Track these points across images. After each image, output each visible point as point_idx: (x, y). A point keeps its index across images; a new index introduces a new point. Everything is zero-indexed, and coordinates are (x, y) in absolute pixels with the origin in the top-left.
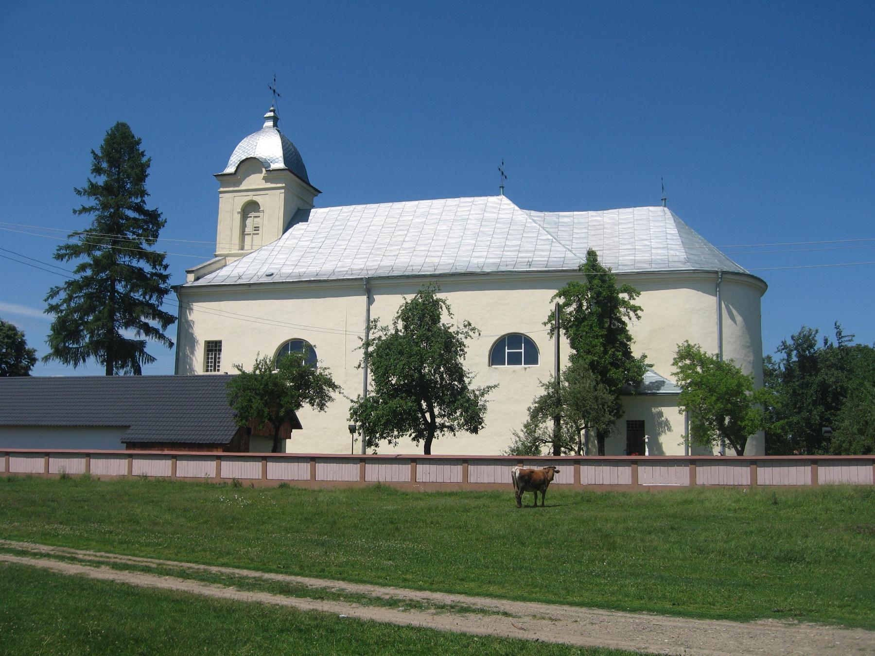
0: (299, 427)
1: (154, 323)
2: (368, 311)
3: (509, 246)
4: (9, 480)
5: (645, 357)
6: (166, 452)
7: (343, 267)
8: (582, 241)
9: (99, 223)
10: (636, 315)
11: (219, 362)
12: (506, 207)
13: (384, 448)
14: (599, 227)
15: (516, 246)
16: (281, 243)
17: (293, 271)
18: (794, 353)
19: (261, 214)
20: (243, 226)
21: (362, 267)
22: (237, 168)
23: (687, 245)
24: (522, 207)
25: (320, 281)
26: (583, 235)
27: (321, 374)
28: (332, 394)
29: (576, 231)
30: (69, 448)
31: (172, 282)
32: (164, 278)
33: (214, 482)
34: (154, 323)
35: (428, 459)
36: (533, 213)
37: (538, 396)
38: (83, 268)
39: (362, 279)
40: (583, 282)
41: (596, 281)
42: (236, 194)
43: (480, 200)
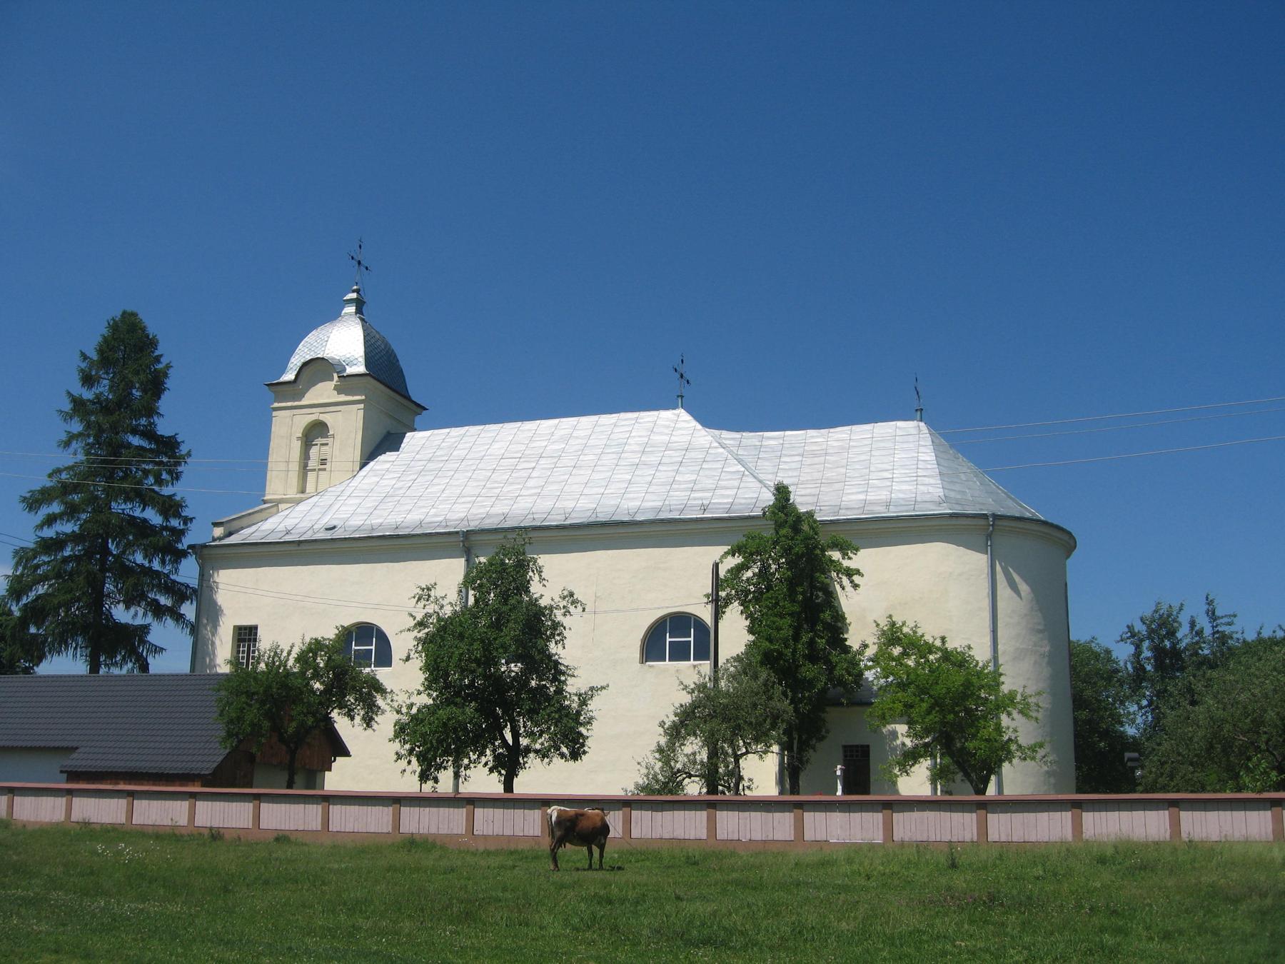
0: (346, 753)
3: (680, 483)
4: (277, 839)
6: (121, 787)
8: (790, 474)
10: (852, 582)
12: (687, 425)
15: (690, 482)
18: (1146, 644)
19: (330, 440)
20: (305, 456)
21: (462, 515)
25: (398, 536)
33: (184, 832)
34: (165, 601)
35: (509, 801)
38: (50, 520)
40: (769, 533)
42: (296, 411)
43: (648, 417)
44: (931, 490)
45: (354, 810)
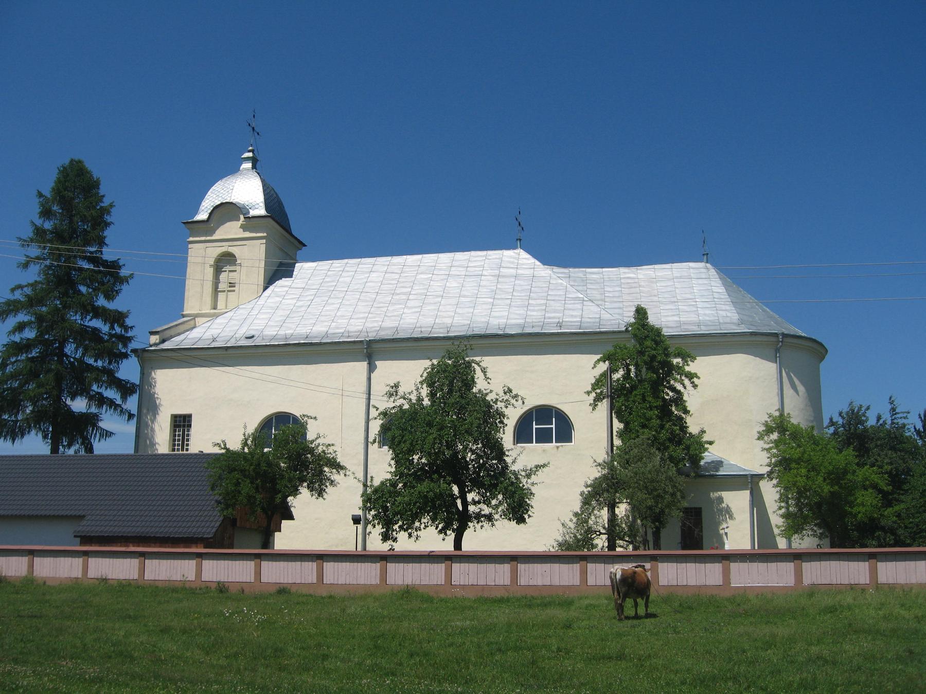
0: (291, 517)
1: (111, 393)
2: (369, 379)
5: (703, 432)
6: (132, 549)
7: (338, 328)
9: (46, 274)
10: (693, 383)
11: (188, 440)
12: (525, 261)
13: (404, 543)
16: (262, 301)
17: (282, 333)
19: (238, 268)
21: (360, 328)
22: (211, 214)
24: (544, 264)
25: (311, 344)
26: (617, 294)
27: (324, 452)
28: (335, 477)
29: (607, 289)
30: (8, 544)
31: (133, 345)
32: (126, 340)
33: (193, 586)
34: (111, 393)
36: (556, 269)
37: (592, 478)
38: (21, 327)
39: (361, 342)
40: (632, 344)
41: (648, 343)
43: (494, 255)
44: (729, 314)
45: (410, 567)
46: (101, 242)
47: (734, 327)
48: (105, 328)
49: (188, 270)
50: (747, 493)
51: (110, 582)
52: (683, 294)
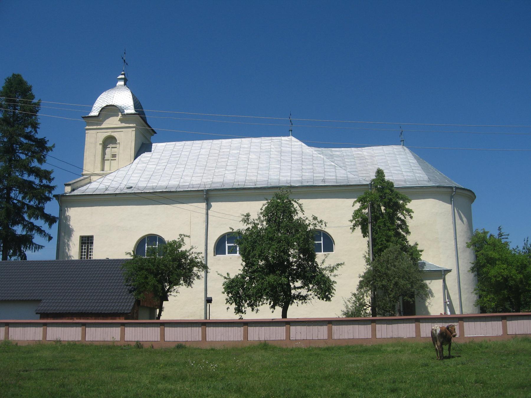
0: (167, 300)
5: (417, 244)
7: (185, 182)
12: (296, 143)
14: (362, 158)
16: (134, 166)
17: (152, 183)
19: (118, 146)
20: (104, 154)
21: (199, 182)
23: (426, 170)
25: (171, 192)
26: (353, 163)
30: (10, 319)
31: (54, 192)
32: (51, 189)
33: (119, 344)
34: (39, 222)
45: (179, 329)
46: (35, 126)
47: (426, 183)
48: (37, 181)
49: (86, 147)
50: (442, 281)
51: (63, 343)
52: (398, 164)
